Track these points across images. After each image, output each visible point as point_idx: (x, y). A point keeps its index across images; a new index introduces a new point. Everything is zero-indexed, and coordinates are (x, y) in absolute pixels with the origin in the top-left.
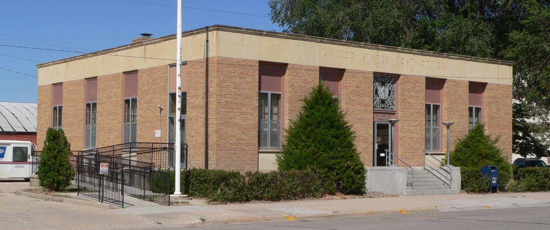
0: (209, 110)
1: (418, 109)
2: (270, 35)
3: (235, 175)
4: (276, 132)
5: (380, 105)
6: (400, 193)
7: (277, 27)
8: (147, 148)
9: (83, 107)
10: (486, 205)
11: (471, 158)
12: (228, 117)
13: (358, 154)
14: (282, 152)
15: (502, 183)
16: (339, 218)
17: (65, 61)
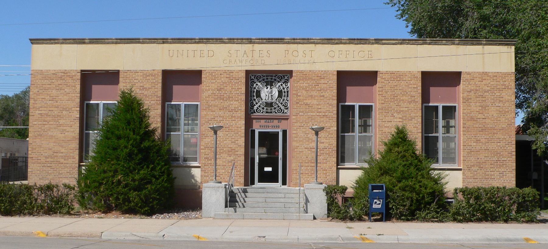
1: (323, 112)
2: (94, 42)
12: (42, 130)
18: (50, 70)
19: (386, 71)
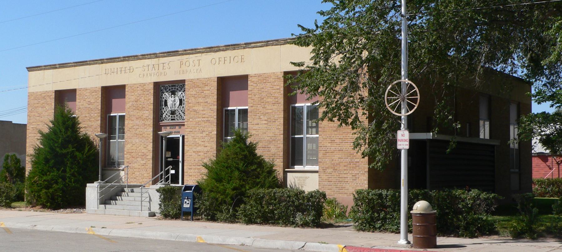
1: (207, 117)
2: (61, 67)
18: (38, 92)
19: (255, 74)
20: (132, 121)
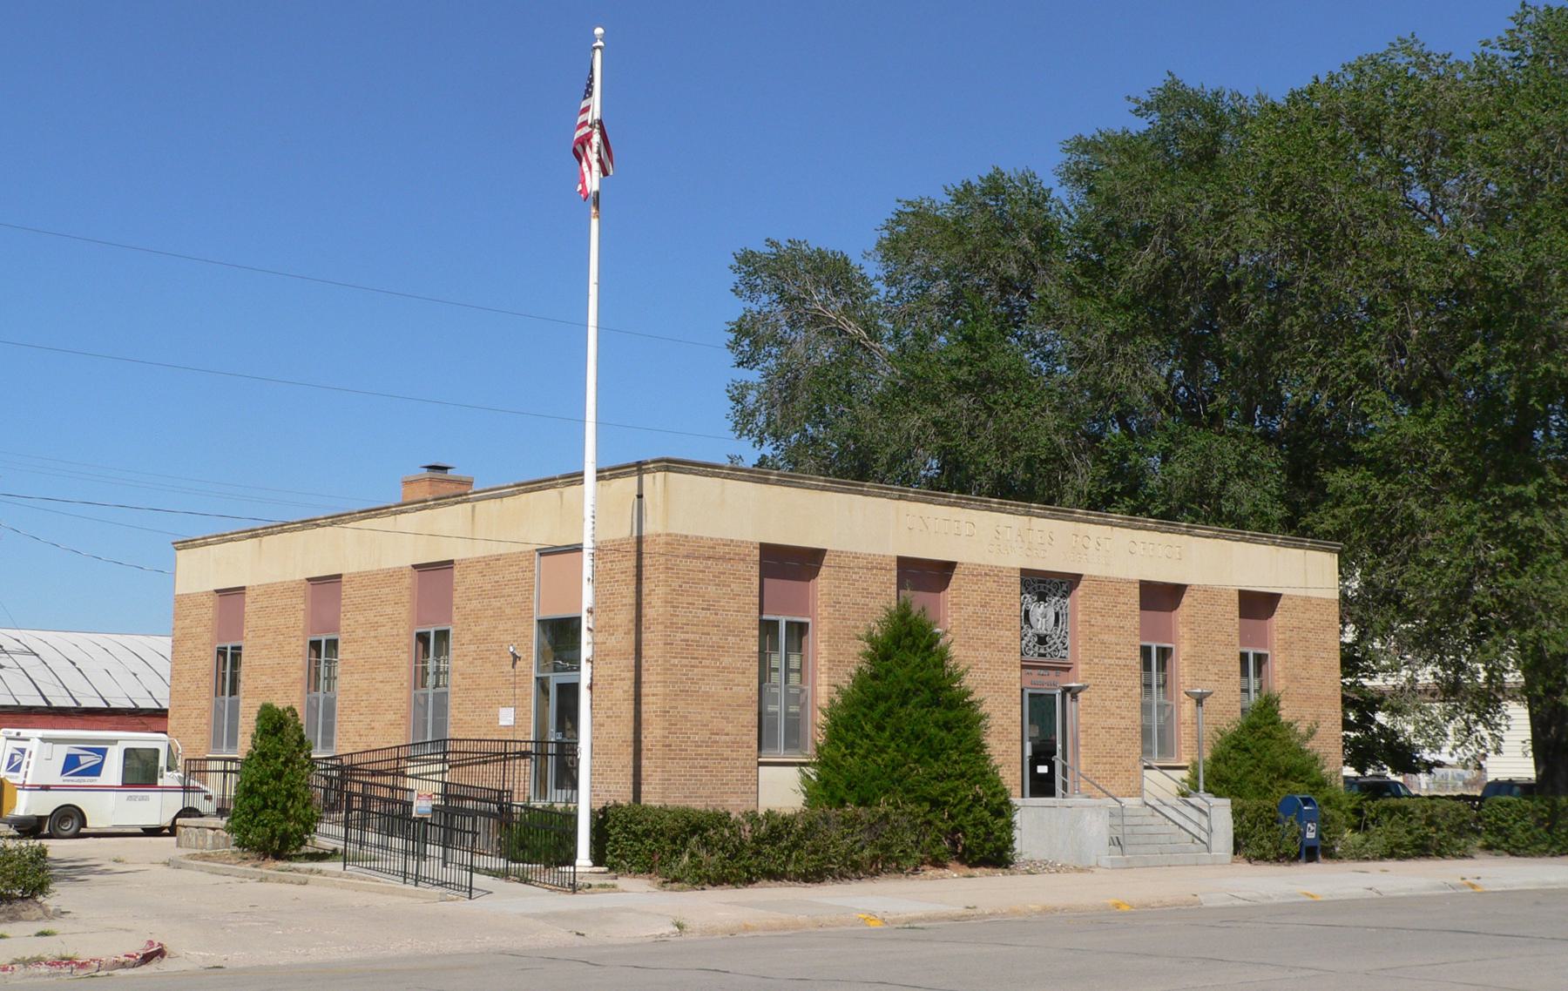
0: (643, 661)
3: (721, 819)
4: (798, 714)
5: (1036, 649)
6: (1093, 863)
7: (750, 454)
8: (477, 753)
9: (300, 650)
10: (1308, 892)
11: (1251, 777)
12: (689, 679)
13: (996, 767)
14: (814, 763)
15: (1330, 838)
16: (980, 921)
17: (254, 534)
20: (974, 650)
